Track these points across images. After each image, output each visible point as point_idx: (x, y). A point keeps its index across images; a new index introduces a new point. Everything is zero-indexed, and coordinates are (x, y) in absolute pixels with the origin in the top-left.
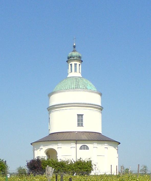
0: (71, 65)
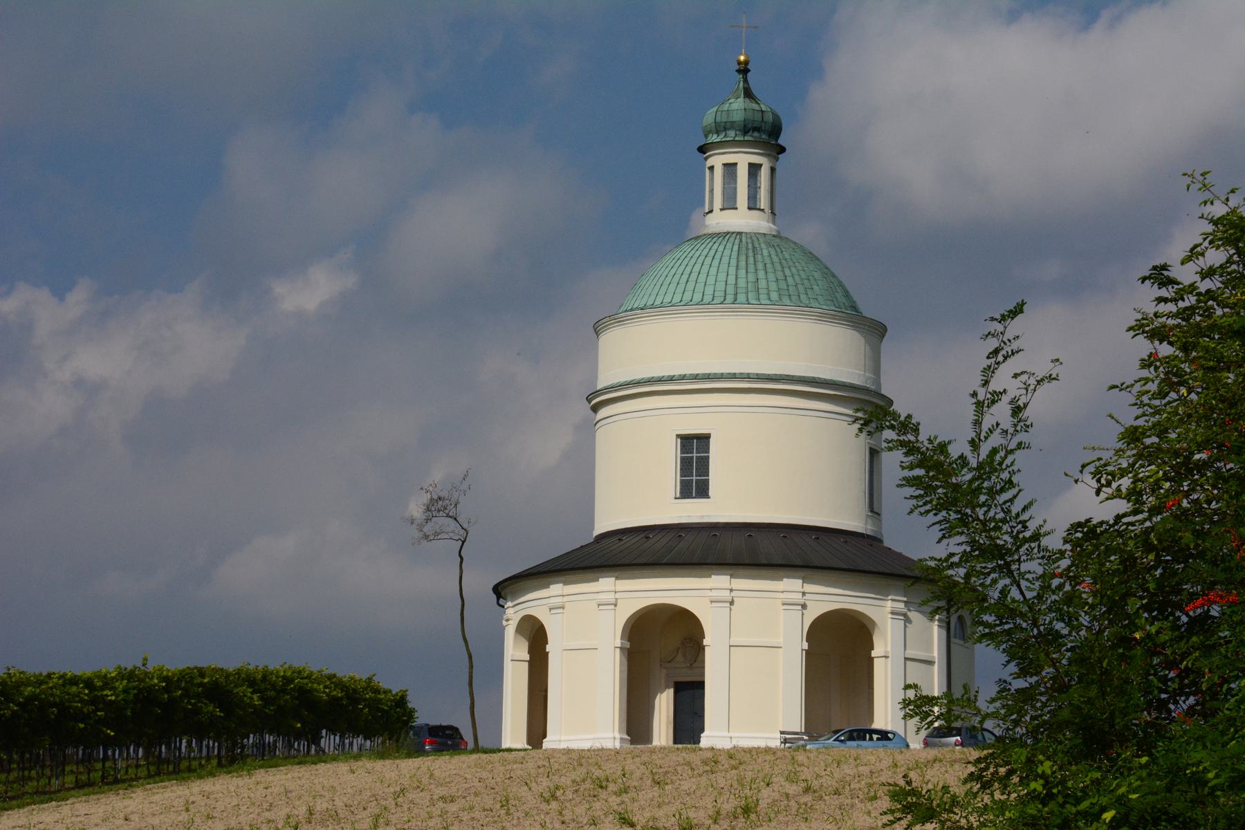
0: (712, 168)
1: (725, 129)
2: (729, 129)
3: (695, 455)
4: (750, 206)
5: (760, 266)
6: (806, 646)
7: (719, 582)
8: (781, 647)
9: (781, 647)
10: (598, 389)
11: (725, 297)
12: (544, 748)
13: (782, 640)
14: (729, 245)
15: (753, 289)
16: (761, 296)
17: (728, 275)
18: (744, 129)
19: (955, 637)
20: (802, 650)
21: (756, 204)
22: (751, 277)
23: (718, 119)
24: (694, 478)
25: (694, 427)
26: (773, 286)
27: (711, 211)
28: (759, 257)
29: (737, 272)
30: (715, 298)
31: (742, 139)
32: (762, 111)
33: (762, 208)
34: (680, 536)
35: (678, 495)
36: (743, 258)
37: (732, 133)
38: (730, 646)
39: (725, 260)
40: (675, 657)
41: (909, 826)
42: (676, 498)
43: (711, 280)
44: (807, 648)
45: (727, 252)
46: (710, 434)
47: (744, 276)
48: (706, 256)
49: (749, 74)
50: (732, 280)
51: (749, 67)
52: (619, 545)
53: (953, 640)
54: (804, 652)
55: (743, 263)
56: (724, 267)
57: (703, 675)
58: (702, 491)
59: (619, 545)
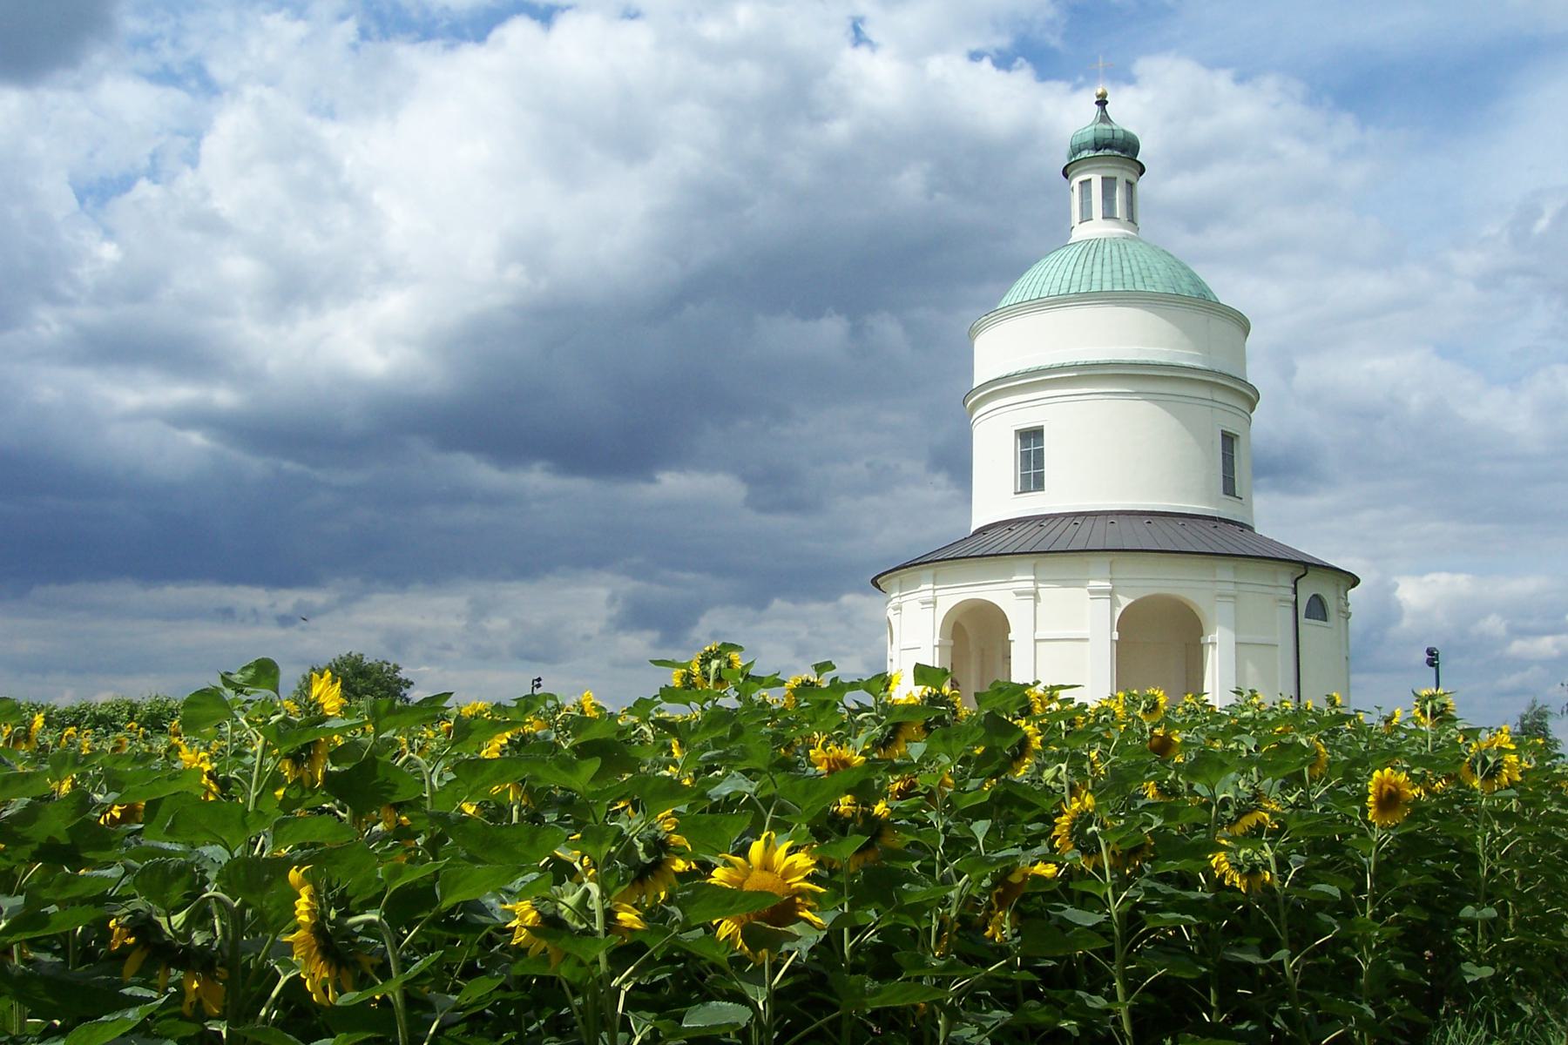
3: (1032, 448)
4: (1106, 216)
5: (1098, 261)
6: (1116, 636)
7: (1024, 581)
8: (1087, 640)
9: (1087, 640)
19: (1307, 616)
20: (1112, 640)
21: (1113, 214)
24: (1032, 471)
25: (1028, 420)
28: (1099, 254)
29: (1102, 276)
32: (1113, 130)
34: (1076, 524)
35: (1019, 490)
37: (1085, 154)
38: (1036, 641)
39: (1067, 260)
42: (1015, 493)
46: (1043, 426)
48: (1075, 265)
49: (1107, 106)
51: (1107, 99)
52: (1010, 534)
58: (1039, 484)
59: (1010, 534)
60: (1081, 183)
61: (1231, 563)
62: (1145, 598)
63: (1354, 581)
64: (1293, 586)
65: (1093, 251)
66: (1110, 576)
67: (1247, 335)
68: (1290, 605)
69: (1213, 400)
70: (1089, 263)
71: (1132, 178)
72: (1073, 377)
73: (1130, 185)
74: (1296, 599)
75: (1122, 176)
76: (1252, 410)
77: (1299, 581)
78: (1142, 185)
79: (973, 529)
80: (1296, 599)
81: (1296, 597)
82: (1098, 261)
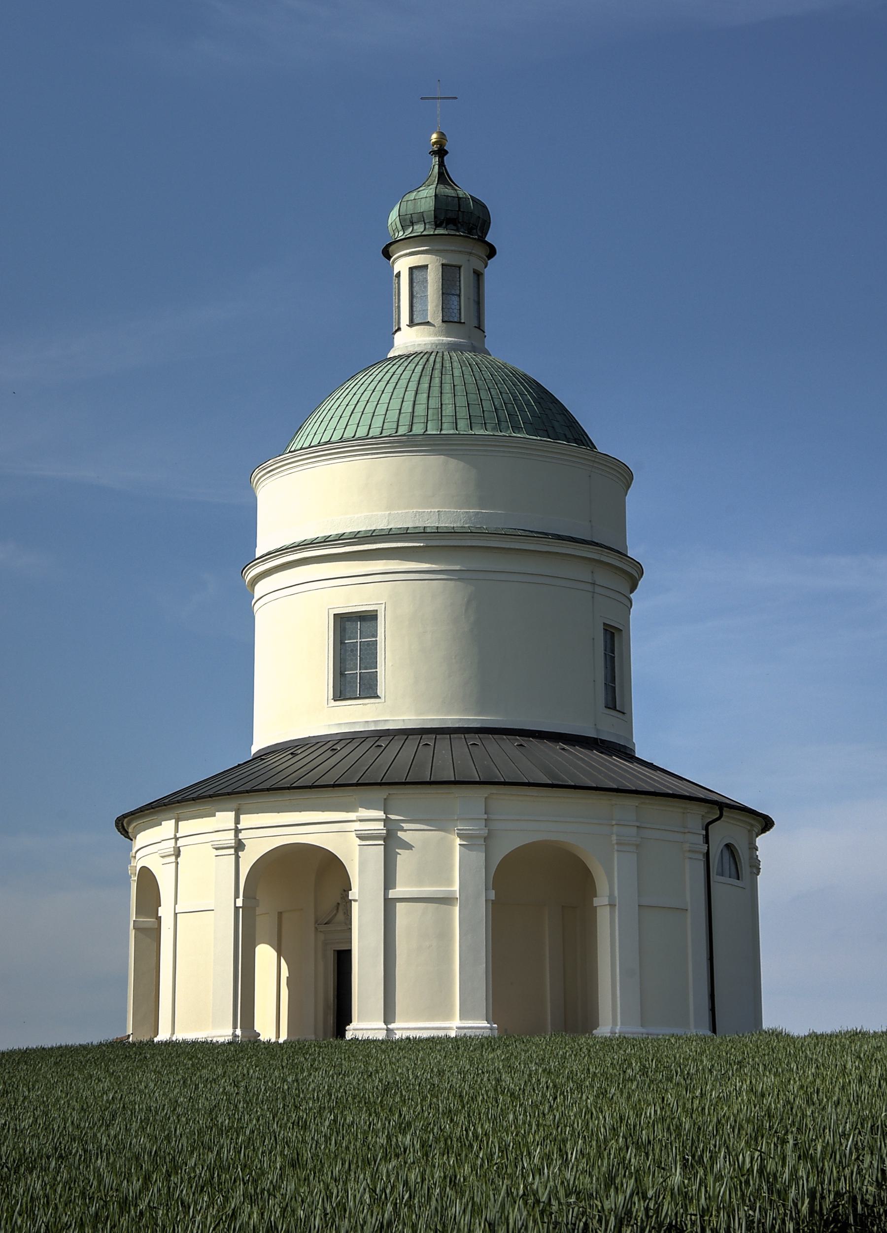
1: (412, 224)
2: (417, 223)
5: (447, 388)
6: (492, 895)
10: (256, 557)
11: (397, 428)
12: (349, 1035)
13: (456, 887)
14: (412, 366)
15: (435, 417)
16: (445, 426)
17: (403, 401)
18: (435, 222)
19: (722, 874)
22: (434, 403)
23: (403, 212)
26: (463, 413)
27: (399, 329)
28: (447, 378)
30: (384, 431)
31: (432, 233)
33: (462, 321)
36: (426, 380)
37: (419, 229)
38: (176, 914)
39: (402, 383)
40: (336, 915)
41: (66, 1232)
43: (381, 410)
44: (494, 899)
45: (407, 374)
46: (377, 611)
47: (426, 401)
50: (407, 407)
53: (714, 877)
54: (490, 905)
55: (425, 386)
56: (400, 392)
57: (349, 941)
60: (411, 269)
61: (631, 802)
62: (534, 842)
63: (767, 824)
64: (704, 832)
65: (437, 373)
66: (485, 817)
67: (629, 487)
68: (701, 857)
69: (471, 532)
70: (435, 391)
71: (477, 264)
72: (420, 546)
73: (478, 275)
74: (708, 850)
75: (467, 263)
76: (633, 588)
77: (710, 827)
78: (492, 271)
79: (254, 749)
80: (708, 850)
81: (708, 847)
82: (447, 388)
